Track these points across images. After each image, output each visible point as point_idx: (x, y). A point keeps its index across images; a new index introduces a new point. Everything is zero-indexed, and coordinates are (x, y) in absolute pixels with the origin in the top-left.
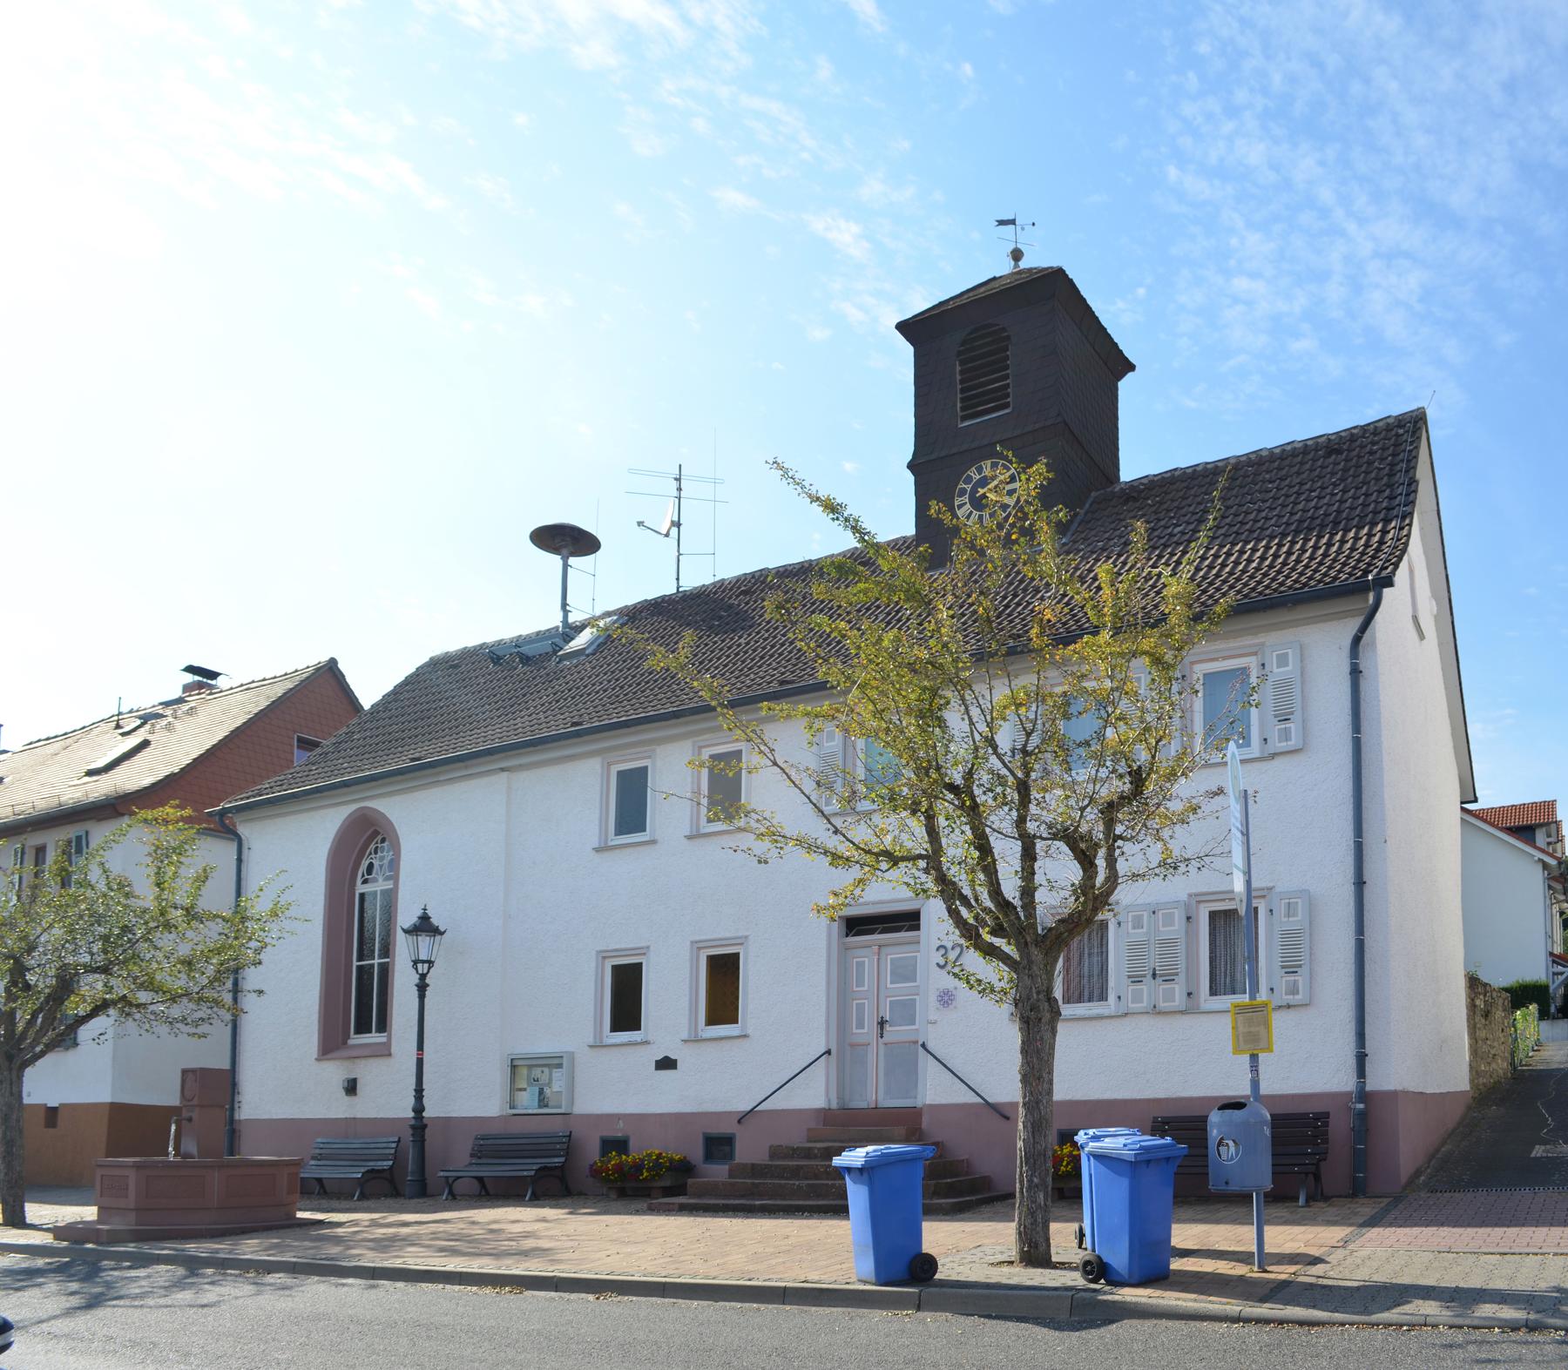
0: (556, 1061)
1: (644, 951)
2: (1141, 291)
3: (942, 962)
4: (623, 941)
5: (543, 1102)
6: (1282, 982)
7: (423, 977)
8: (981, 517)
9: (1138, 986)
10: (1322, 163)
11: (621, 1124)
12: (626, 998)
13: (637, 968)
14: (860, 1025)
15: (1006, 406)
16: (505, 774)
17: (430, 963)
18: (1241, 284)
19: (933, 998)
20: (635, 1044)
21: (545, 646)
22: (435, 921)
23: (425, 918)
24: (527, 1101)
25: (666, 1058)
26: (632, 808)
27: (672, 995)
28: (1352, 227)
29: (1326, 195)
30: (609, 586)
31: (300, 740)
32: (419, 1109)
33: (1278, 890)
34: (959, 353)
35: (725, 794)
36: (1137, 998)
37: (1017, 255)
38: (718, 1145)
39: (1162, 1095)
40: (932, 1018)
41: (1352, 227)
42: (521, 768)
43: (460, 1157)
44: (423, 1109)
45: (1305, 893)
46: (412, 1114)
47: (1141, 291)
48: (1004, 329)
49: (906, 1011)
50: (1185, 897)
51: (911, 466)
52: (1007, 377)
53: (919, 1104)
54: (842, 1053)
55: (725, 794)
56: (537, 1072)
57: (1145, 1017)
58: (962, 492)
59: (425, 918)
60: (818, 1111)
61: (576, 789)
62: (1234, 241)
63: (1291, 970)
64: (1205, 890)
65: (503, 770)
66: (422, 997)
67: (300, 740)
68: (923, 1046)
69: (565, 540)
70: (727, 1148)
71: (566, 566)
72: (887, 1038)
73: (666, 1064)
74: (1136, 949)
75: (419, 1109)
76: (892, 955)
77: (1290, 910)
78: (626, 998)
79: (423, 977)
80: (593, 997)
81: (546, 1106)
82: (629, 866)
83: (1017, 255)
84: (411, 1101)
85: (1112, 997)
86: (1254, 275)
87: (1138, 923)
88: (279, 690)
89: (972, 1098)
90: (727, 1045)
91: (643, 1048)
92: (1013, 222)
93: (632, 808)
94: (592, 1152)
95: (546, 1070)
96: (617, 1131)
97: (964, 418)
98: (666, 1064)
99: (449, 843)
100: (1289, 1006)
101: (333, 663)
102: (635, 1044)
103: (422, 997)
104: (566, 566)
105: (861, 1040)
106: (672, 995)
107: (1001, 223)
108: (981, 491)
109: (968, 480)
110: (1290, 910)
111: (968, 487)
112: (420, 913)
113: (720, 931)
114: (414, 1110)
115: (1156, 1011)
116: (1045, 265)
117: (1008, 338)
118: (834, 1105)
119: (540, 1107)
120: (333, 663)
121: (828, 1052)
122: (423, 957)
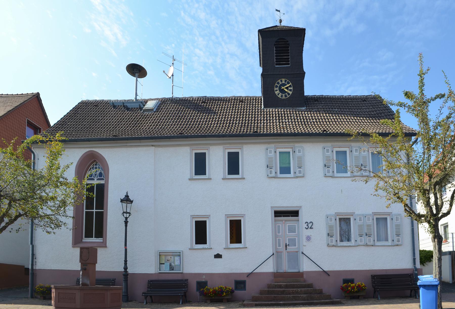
0: (178, 254)
1: (208, 217)
2: (173, 45)
3: (307, 227)
4: (201, 212)
5: (172, 268)
6: (396, 238)
7: (126, 218)
8: (282, 95)
9: (361, 238)
10: (217, 24)
11: (204, 277)
12: (201, 232)
13: (205, 222)
14: (280, 246)
15: (289, 64)
16: (154, 147)
17: (129, 213)
18: (197, 51)
19: (304, 238)
20: (206, 249)
21: (137, 106)
22: (131, 198)
23: (127, 196)
24: (166, 269)
25: (218, 254)
26: (200, 166)
27: (218, 232)
28: (223, 44)
29: (218, 33)
30: (151, 90)
31: (29, 122)
32: (126, 268)
33: (393, 213)
34: (275, 45)
35: (233, 165)
36: (361, 241)
37: (281, 21)
38: (240, 284)
39: (368, 269)
40: (304, 244)
41: (223, 44)
42: (159, 146)
43: (140, 289)
44: (127, 269)
45: (182, 251)
46: (123, 270)
47: (173, 45)
48: (287, 41)
49: (293, 242)
50: (371, 213)
51: (305, 73)
52: (288, 56)
53: (301, 271)
54: (277, 255)
55: (233, 165)
56: (169, 258)
57: (363, 247)
58: (277, 87)
59: (127, 196)
60: (272, 273)
61: (181, 157)
62: (196, 38)
63: (398, 235)
64: (376, 212)
65: (152, 146)
66: (126, 226)
67: (29, 122)
68: (302, 253)
69: (136, 70)
70: (242, 285)
71: (137, 80)
72: (288, 250)
73: (218, 256)
74: (360, 227)
75: (126, 268)
76: (288, 224)
77: (397, 219)
78: (201, 232)
79: (126, 218)
80: (190, 232)
81: (173, 270)
82: (200, 186)
83: (281, 21)
84: (123, 265)
85: (353, 241)
86: (200, 50)
87: (360, 220)
88: (21, 100)
89: (318, 269)
90: (240, 250)
91: (209, 250)
92: (279, 11)
93: (200, 166)
94: (193, 286)
95: (172, 257)
96: (203, 279)
97: (276, 64)
98: (218, 256)
99: (129, 169)
100: (397, 245)
101: (38, 94)
102: (206, 249)
103: (126, 226)
104: (137, 80)
105: (280, 251)
106: (218, 232)
107: (277, 10)
108: (283, 88)
109: (278, 83)
110: (397, 219)
111: (278, 85)
112: (125, 194)
113: (235, 212)
114: (124, 268)
115: (367, 245)
116: (296, 26)
117: (289, 44)
118: (276, 272)
119: (170, 270)
120: (38, 94)
121: (273, 254)
122: (128, 211)
